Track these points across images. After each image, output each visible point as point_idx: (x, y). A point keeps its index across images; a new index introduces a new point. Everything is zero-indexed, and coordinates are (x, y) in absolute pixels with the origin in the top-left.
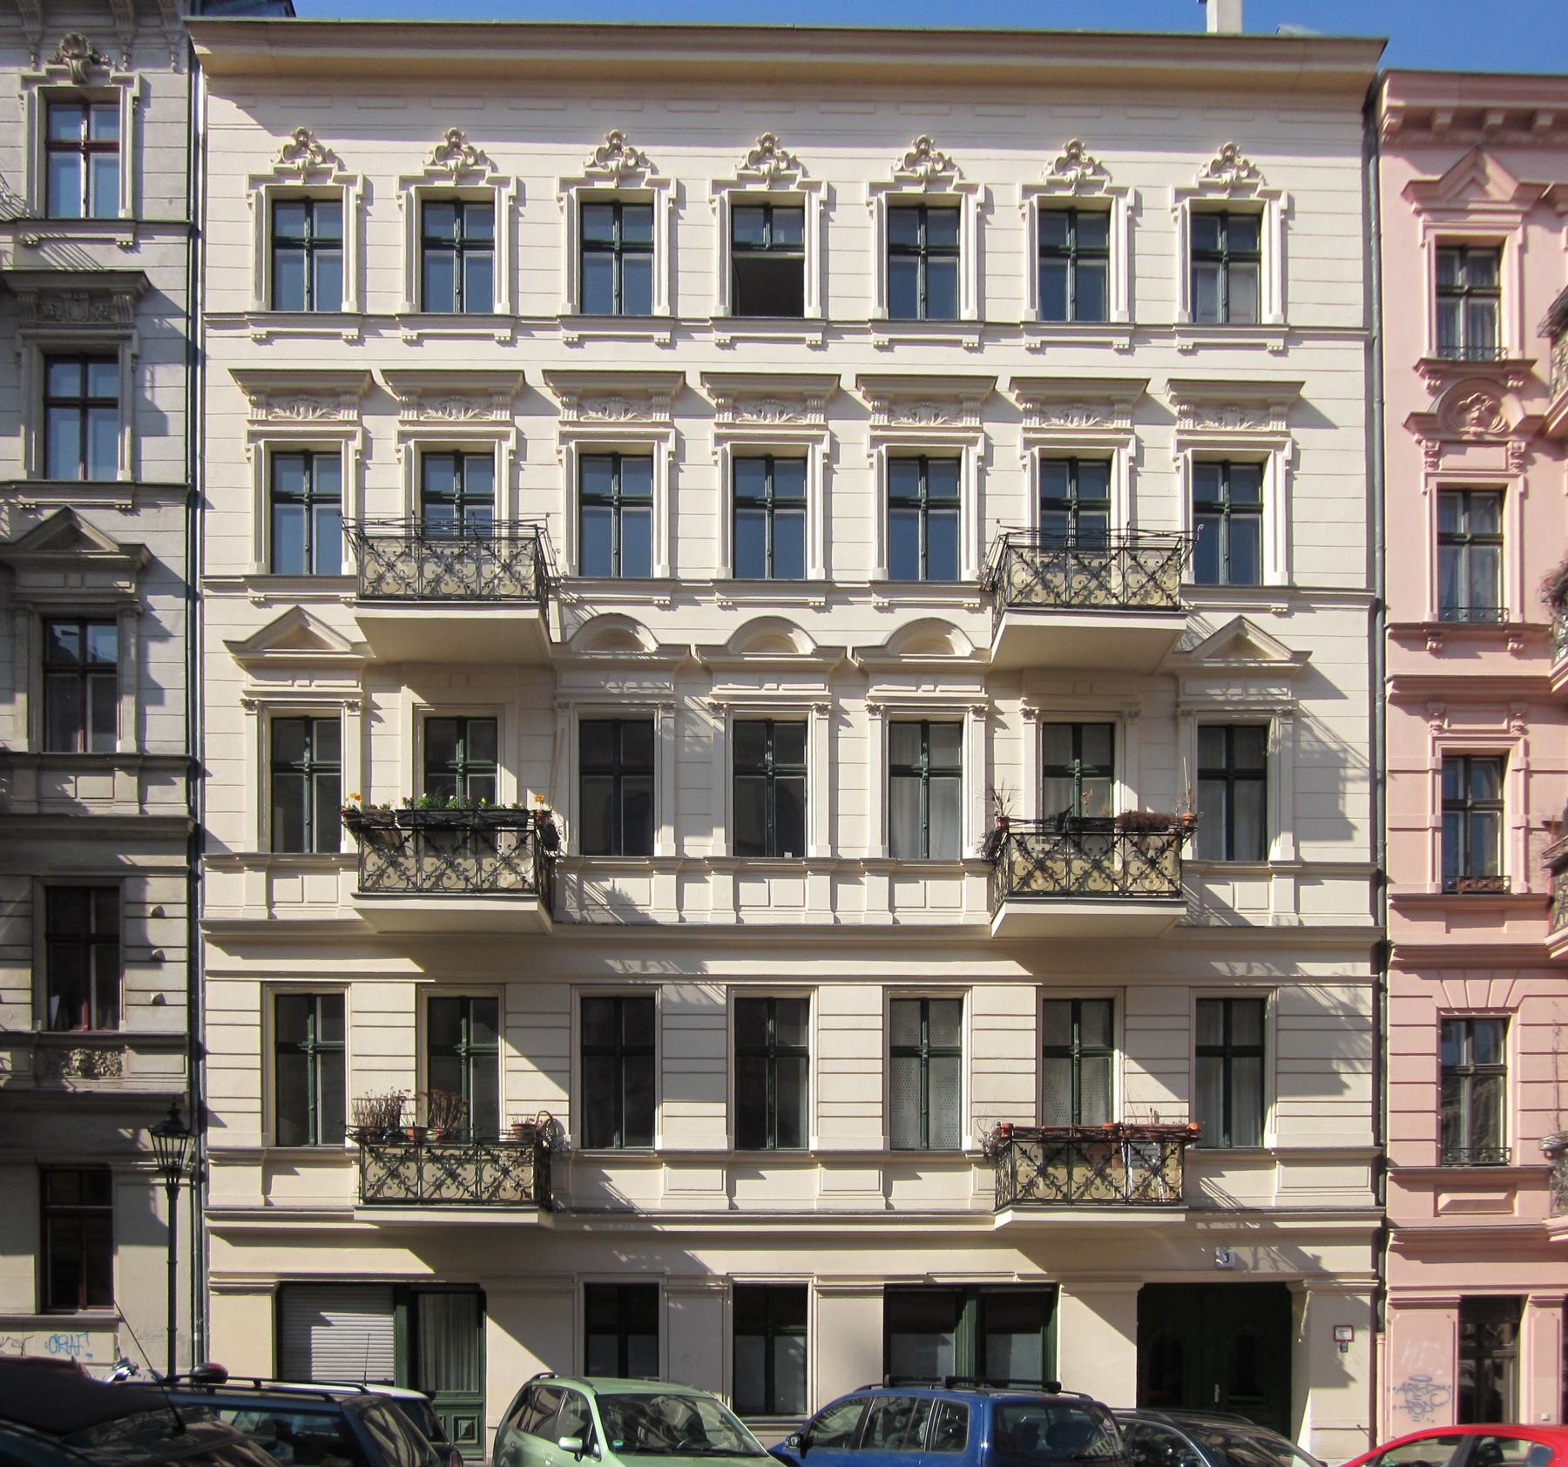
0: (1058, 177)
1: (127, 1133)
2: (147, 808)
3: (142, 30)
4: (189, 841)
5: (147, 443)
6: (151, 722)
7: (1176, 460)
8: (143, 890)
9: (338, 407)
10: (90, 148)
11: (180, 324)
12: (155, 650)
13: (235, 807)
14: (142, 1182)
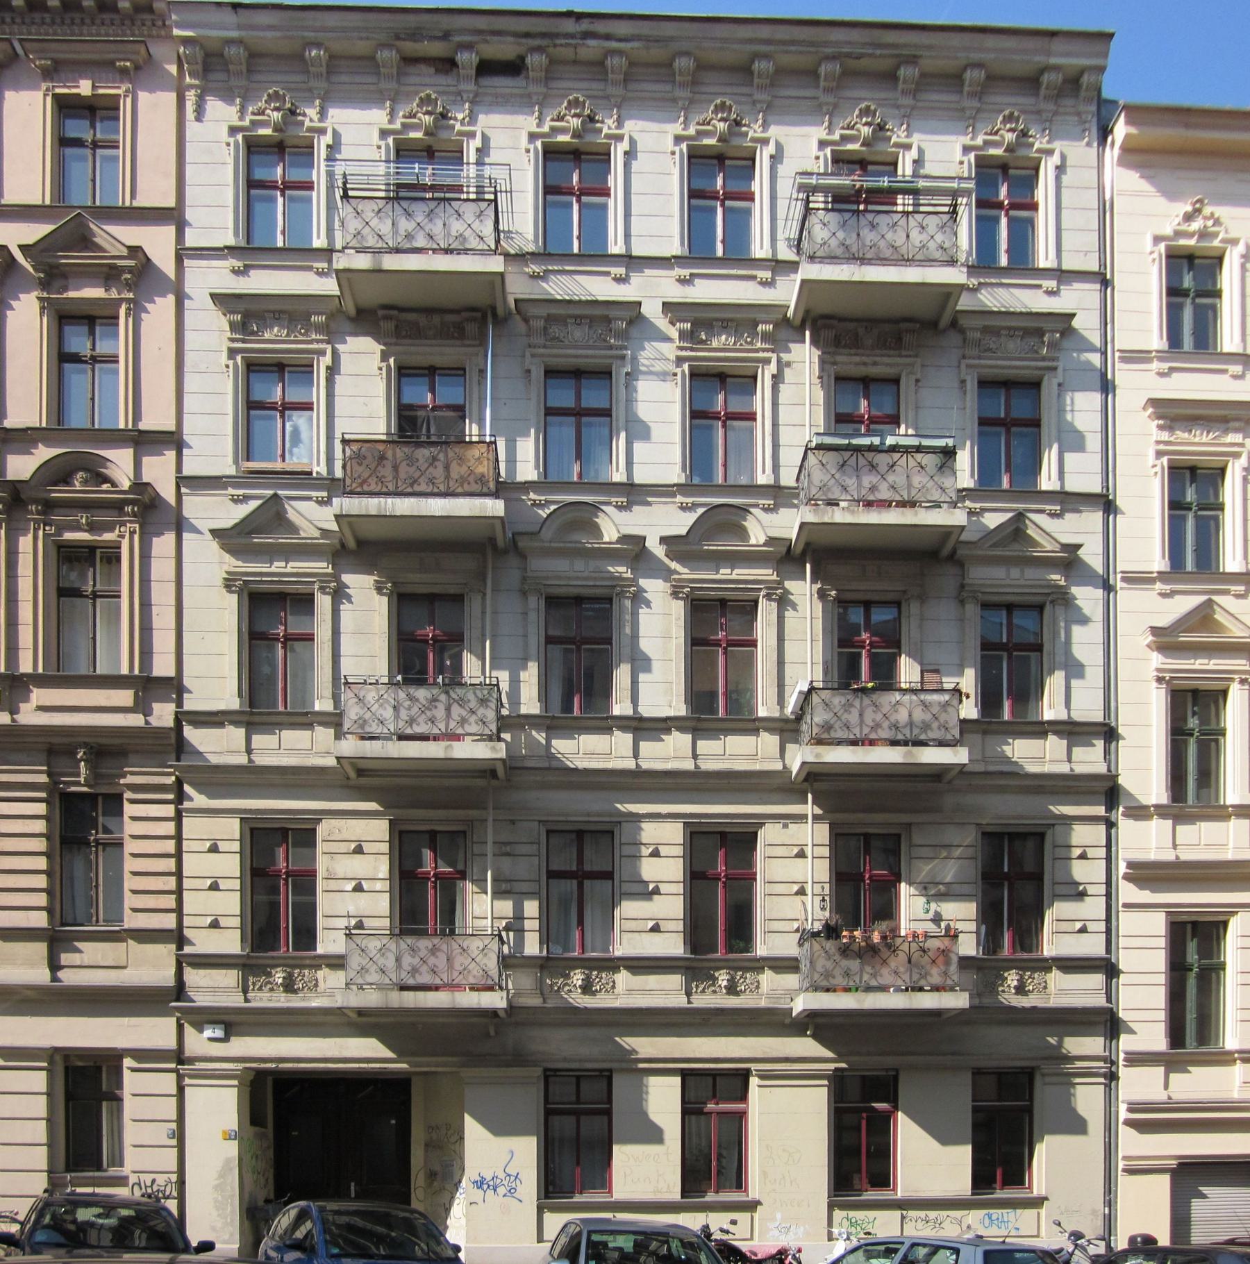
0: (1184, 227)
1: (1052, 1041)
2: (641, 762)
3: (1061, 110)
4: (1106, 793)
5: (638, 447)
6: (642, 688)
7: (1154, 466)
8: (1068, 835)
9: (1226, 431)
10: (287, 186)
11: (1095, 359)
12: (1077, 630)
13: (1144, 767)
14: (1066, 1081)
